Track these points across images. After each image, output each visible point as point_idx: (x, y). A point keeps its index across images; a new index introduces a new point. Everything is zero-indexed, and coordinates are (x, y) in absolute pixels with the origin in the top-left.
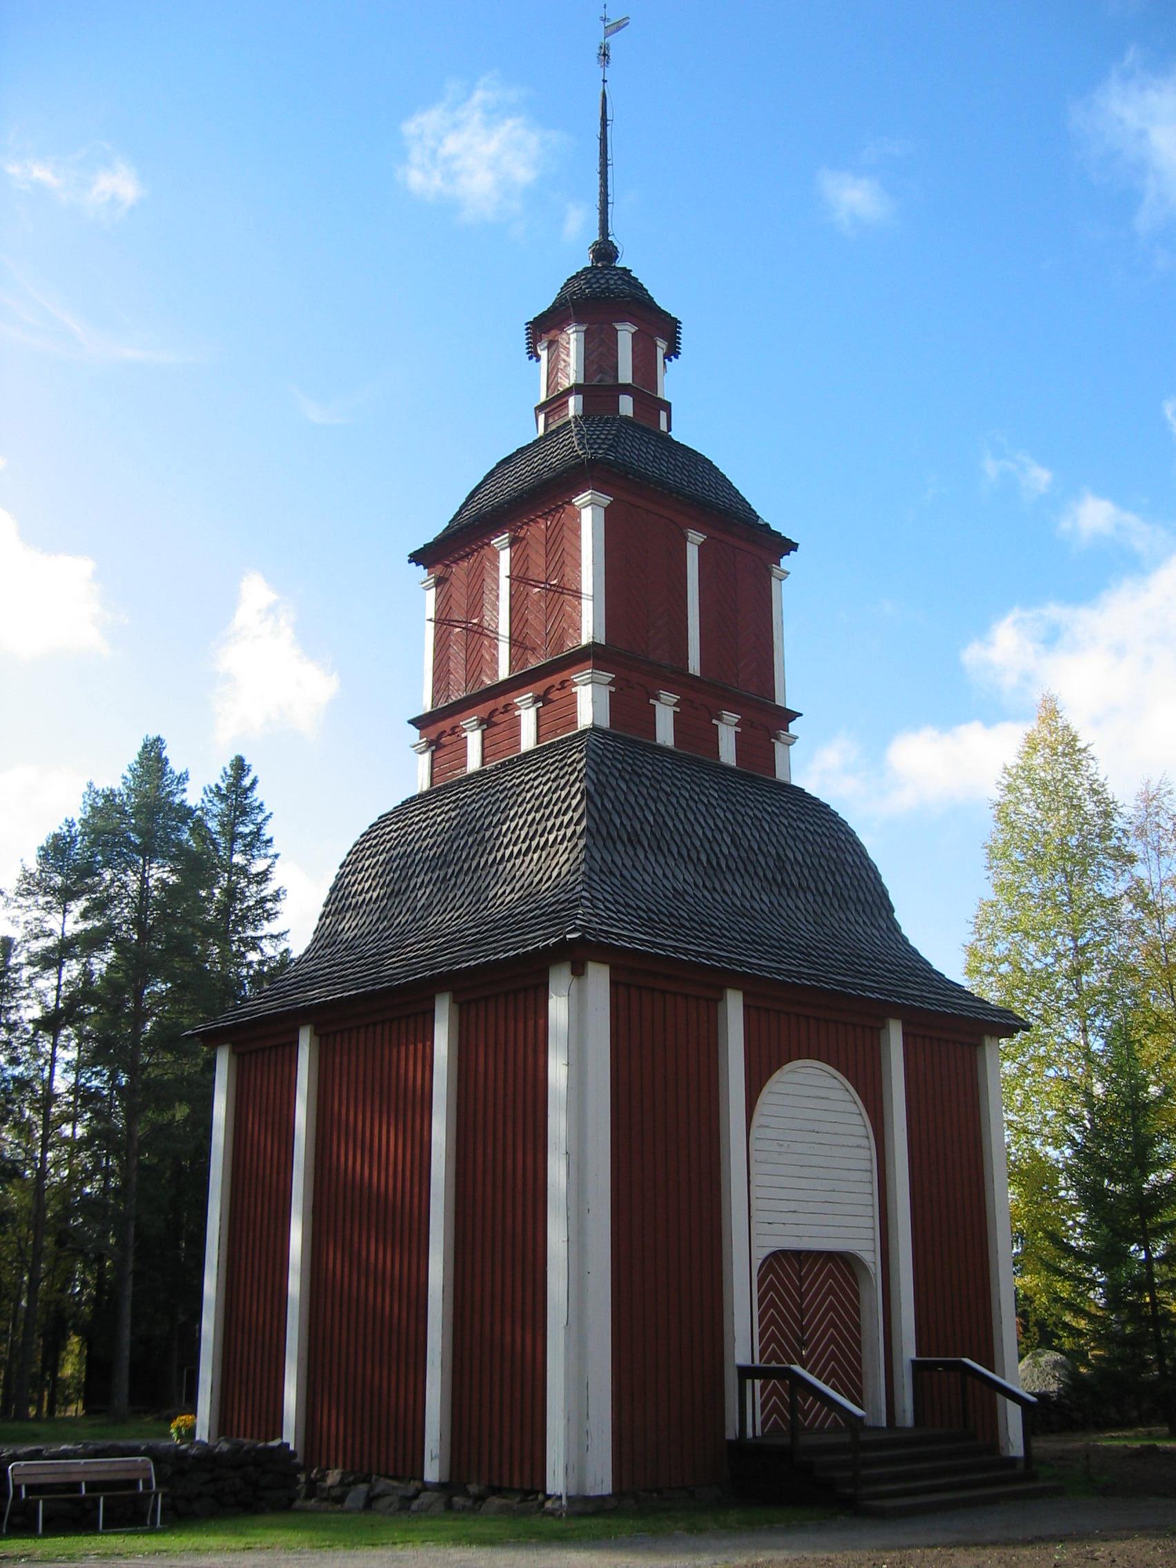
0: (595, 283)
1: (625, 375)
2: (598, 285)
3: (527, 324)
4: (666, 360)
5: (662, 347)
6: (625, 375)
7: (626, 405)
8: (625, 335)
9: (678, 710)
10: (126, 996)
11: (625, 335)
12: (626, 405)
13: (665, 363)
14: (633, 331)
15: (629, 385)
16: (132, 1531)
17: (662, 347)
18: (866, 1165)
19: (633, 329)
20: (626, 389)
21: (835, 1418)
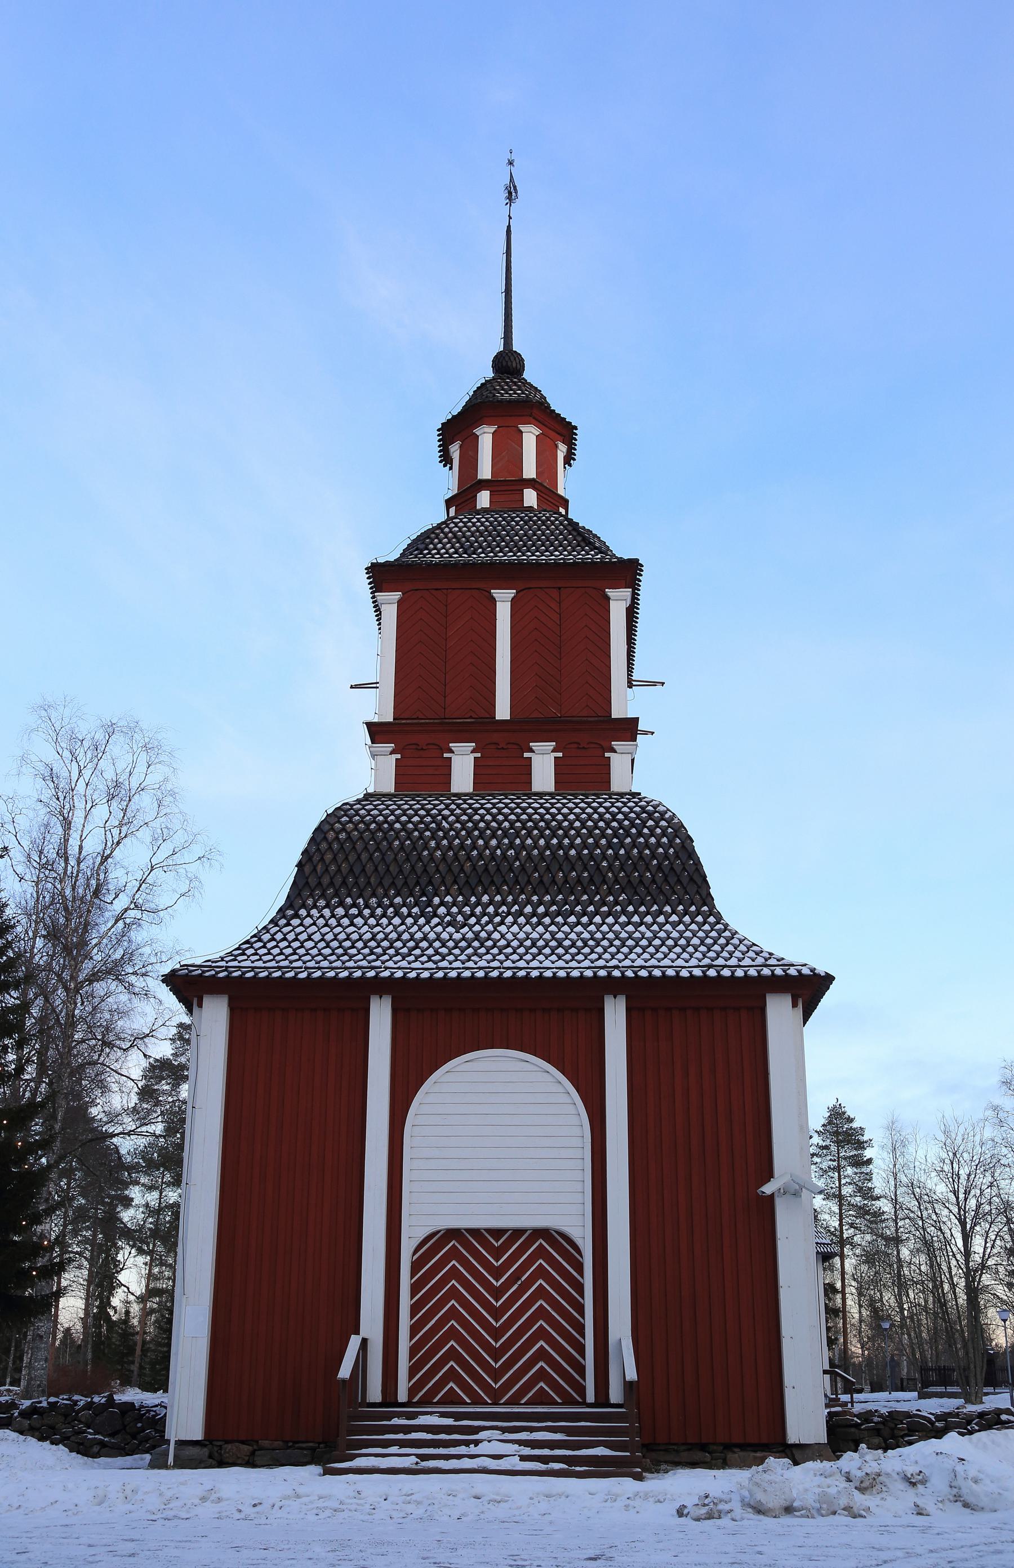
0: (270, 941)
1: (530, 471)
2: (274, 943)
3: (366, 569)
4: (566, 466)
5: (562, 450)
6: (530, 471)
7: (530, 498)
8: (530, 436)
9: (560, 755)
10: (46, 1243)
11: (530, 436)
12: (530, 498)
13: (565, 468)
14: (538, 433)
15: (533, 480)
16: (128, 1464)
17: (562, 450)
18: (578, 1153)
19: (537, 431)
20: (531, 483)
21: (496, 1385)
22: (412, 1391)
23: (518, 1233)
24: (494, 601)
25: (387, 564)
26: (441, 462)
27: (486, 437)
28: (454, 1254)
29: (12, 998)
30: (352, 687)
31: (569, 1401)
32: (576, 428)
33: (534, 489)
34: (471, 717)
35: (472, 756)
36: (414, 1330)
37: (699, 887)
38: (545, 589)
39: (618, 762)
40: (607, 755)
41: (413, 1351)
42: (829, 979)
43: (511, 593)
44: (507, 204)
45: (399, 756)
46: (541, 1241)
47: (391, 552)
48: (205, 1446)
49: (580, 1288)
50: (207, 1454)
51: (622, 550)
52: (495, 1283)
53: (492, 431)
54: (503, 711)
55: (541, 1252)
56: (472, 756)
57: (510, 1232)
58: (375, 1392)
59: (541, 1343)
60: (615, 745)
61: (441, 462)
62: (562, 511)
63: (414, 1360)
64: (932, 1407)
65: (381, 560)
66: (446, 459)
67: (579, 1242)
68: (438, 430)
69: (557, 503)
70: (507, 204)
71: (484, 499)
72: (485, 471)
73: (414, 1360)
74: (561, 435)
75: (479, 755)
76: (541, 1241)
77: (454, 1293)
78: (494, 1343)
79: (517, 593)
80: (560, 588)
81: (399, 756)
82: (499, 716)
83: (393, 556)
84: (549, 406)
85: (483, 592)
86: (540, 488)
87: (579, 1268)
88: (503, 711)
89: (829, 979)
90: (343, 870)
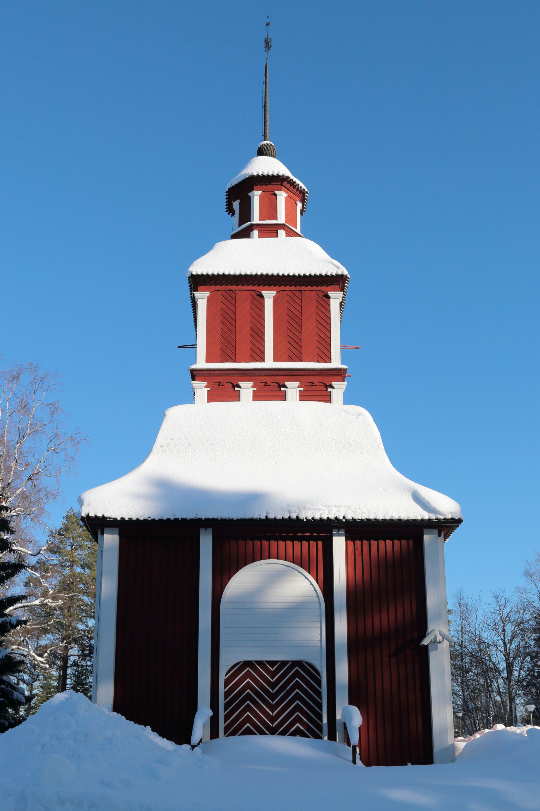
8: (282, 196)
9: (302, 389)
21: (273, 724)
23: (284, 663)
26: (226, 211)
28: (248, 675)
30: (179, 347)
33: (284, 229)
36: (227, 717)
38: (293, 291)
39: (411, 763)
43: (273, 293)
44: (266, 51)
45: (209, 389)
46: (297, 668)
49: (319, 694)
53: (259, 194)
55: (297, 674)
59: (297, 690)
61: (226, 211)
66: (230, 210)
67: (319, 668)
68: (226, 192)
70: (266, 51)
74: (443, 522)
75: (255, 389)
76: (297, 668)
78: (271, 714)
79: (276, 293)
80: (301, 291)
81: (209, 389)
85: (256, 292)
86: (288, 230)
87: (319, 683)
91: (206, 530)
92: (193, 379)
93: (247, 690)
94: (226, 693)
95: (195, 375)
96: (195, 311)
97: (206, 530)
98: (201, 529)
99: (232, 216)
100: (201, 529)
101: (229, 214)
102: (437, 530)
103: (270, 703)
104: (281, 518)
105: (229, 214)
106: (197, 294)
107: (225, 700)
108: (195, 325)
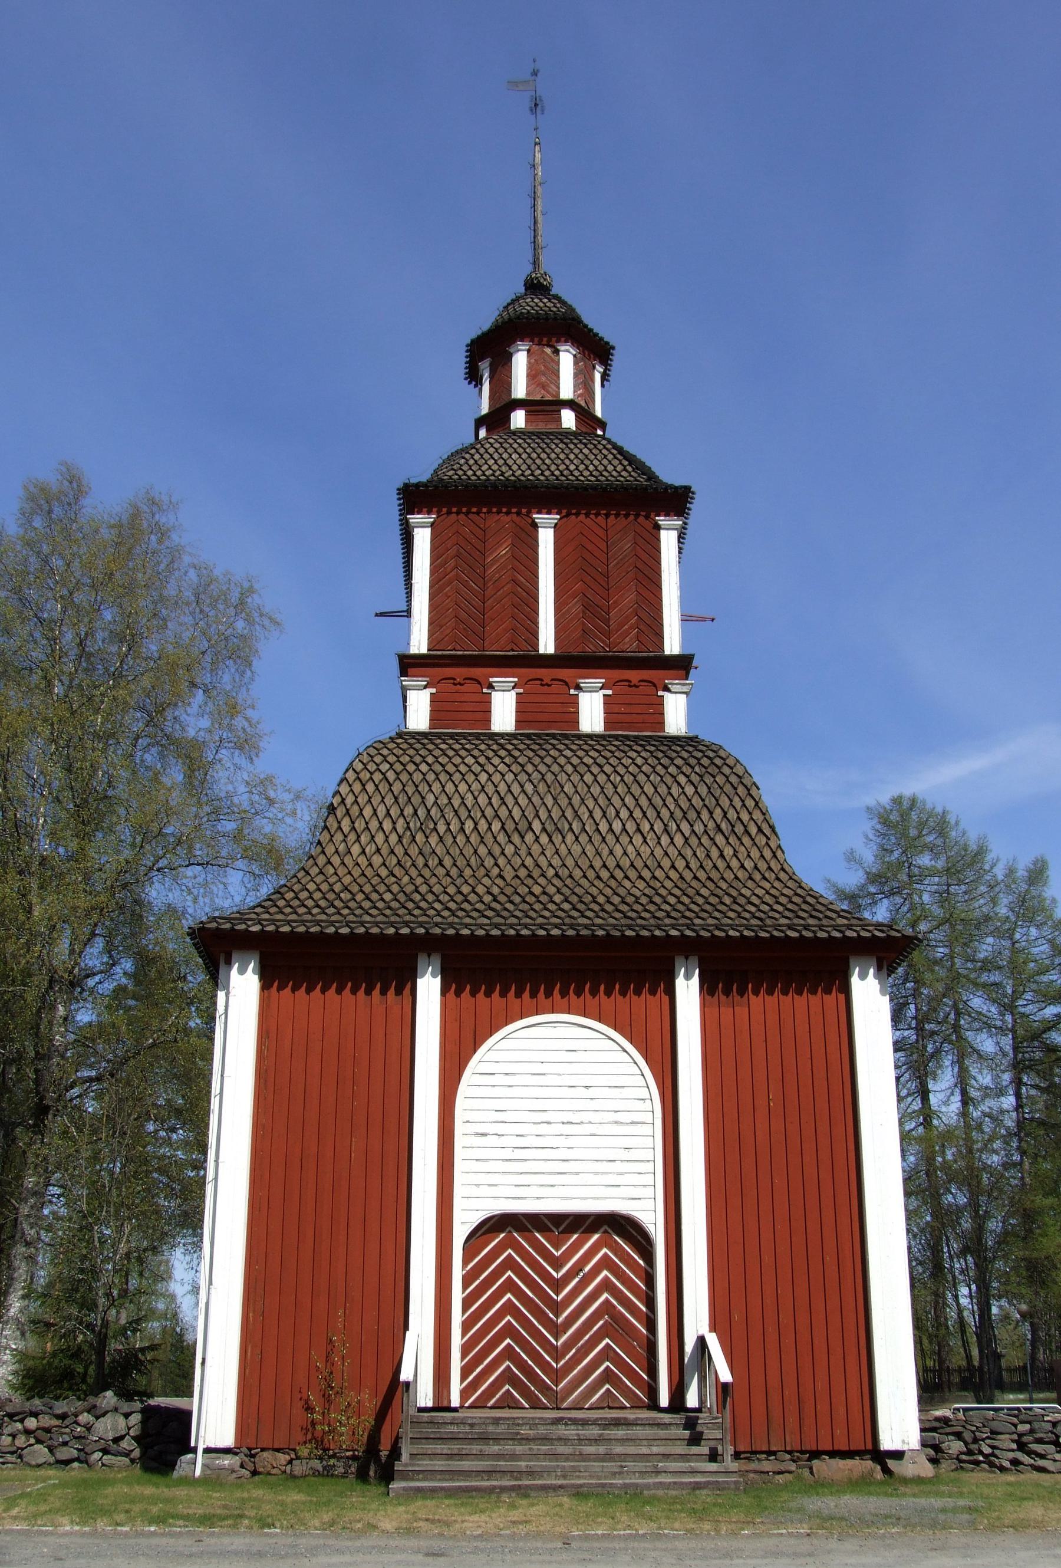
1: (567, 391)
9: (610, 692)
11: (567, 360)
12: (568, 419)
20: (570, 404)
22: (465, 1394)
24: (535, 526)
25: (418, 485)
27: (520, 361)
29: (8, 889)
30: (377, 615)
31: (637, 1406)
32: (613, 348)
33: (573, 410)
34: (513, 650)
35: (513, 693)
36: (466, 1326)
37: (768, 838)
40: (660, 693)
41: (465, 1350)
42: (694, 655)
45: (434, 691)
47: (421, 474)
48: (236, 1454)
50: (239, 1464)
51: (670, 475)
52: (554, 1274)
54: (547, 644)
56: (513, 693)
57: (653, 1384)
58: (425, 1396)
60: (670, 684)
62: (599, 432)
63: (471, 1378)
64: (977, 1317)
65: (414, 481)
66: (474, 377)
67: (650, 1229)
69: (594, 425)
71: (519, 419)
72: (520, 389)
73: (471, 1378)
77: (510, 1285)
81: (434, 691)
82: (542, 651)
83: (424, 478)
84: (580, 321)
86: (578, 410)
88: (547, 644)
89: (694, 655)
90: (379, 814)
91: (429, 956)
92: (404, 672)
93: (507, 1271)
94: (464, 1277)
95: (409, 664)
96: (408, 570)
97: (429, 956)
98: (513, 397)
99: (476, 386)
100: (513, 397)
101: (470, 383)
102: (697, 957)
103: (552, 1297)
104: (973, 847)
105: (470, 383)
106: (414, 519)
107: (463, 1292)
108: (407, 602)
